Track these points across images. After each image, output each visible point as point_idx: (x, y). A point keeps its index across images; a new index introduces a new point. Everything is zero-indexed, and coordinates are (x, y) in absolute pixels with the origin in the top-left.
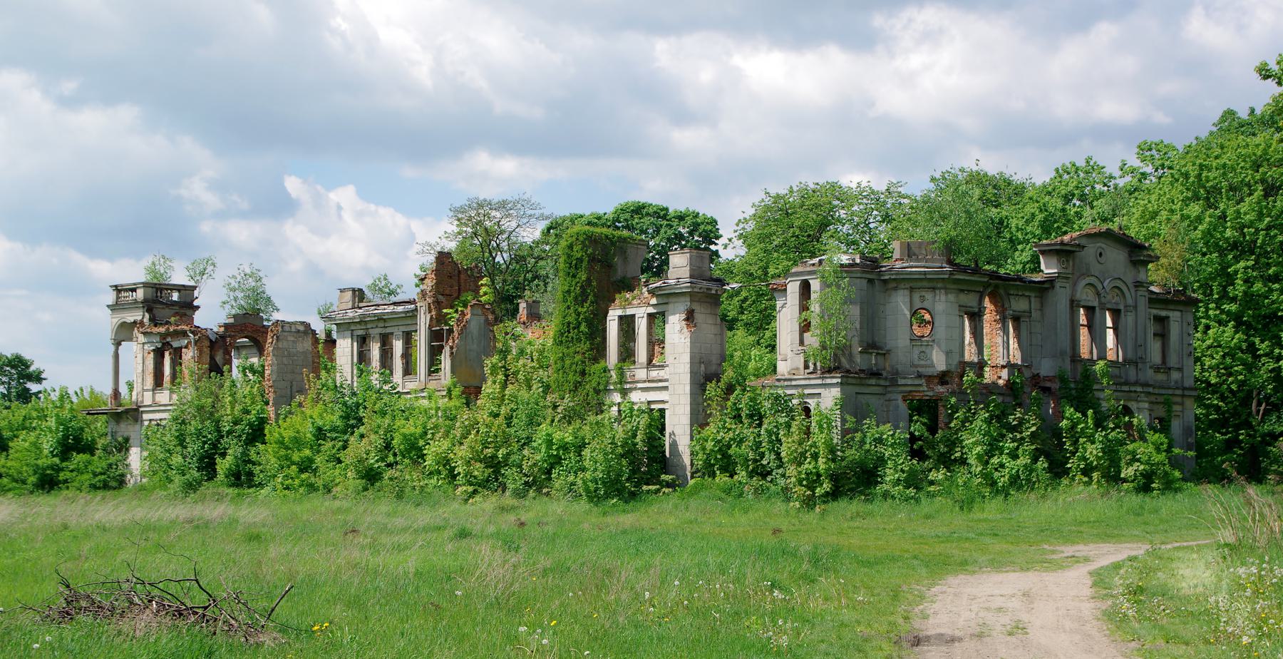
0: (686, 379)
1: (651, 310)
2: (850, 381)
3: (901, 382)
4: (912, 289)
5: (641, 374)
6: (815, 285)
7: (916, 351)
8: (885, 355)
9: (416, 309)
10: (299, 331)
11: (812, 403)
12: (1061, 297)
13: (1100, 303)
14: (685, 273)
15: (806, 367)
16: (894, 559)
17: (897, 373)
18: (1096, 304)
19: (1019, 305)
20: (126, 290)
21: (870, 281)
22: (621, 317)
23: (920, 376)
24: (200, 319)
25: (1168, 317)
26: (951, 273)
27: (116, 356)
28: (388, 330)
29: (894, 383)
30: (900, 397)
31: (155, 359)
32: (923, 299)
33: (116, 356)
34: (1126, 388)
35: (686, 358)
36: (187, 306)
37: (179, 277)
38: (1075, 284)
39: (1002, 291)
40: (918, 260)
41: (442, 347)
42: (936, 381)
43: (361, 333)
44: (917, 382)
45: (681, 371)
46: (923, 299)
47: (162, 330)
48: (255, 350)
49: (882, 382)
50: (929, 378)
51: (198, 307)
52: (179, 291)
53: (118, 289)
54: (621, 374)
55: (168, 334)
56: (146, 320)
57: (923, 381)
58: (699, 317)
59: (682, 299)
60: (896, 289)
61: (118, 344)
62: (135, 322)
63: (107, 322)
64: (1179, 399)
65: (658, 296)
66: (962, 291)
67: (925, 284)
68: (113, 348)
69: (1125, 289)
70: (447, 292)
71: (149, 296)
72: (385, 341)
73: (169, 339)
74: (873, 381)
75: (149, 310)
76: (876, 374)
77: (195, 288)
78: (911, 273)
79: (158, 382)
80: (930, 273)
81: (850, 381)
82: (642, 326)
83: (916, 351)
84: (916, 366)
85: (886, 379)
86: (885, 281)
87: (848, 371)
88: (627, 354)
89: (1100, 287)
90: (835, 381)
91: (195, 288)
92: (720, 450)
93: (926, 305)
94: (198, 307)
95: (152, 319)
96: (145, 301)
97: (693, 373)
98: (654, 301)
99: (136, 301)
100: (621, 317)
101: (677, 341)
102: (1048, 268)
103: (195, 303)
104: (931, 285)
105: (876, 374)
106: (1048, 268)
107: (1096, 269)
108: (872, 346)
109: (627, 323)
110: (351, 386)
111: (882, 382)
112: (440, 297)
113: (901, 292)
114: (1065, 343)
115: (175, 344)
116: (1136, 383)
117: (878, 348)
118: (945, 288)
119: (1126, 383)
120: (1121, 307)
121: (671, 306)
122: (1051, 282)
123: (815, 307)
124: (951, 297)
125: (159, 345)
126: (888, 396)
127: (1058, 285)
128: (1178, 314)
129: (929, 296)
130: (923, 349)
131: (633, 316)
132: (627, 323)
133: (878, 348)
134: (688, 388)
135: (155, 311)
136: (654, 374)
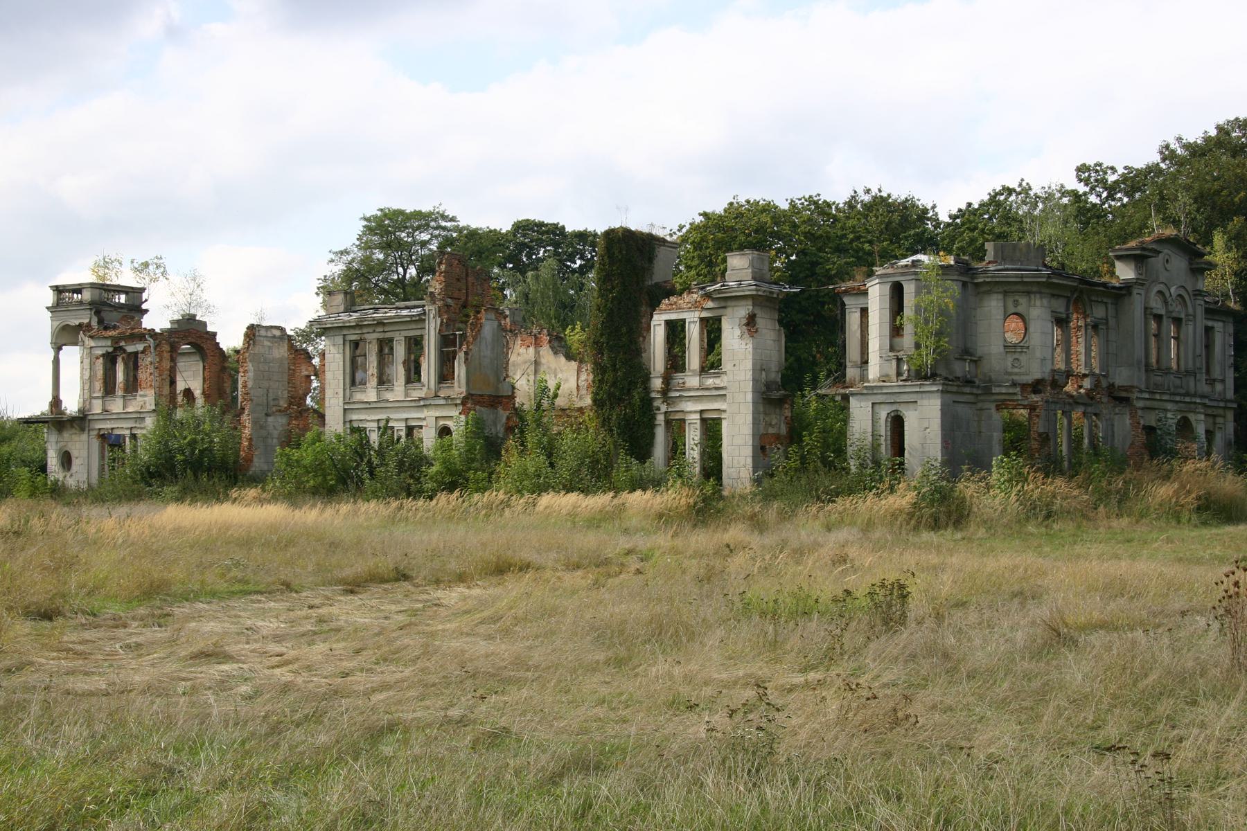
0: (749, 386)
1: (705, 314)
2: (950, 389)
3: (995, 390)
4: (1005, 293)
5: (693, 381)
6: (909, 289)
7: (1010, 359)
8: (976, 362)
9: (425, 314)
10: (274, 337)
11: (138, 432)
12: (1137, 303)
13: (1168, 312)
14: (747, 275)
15: (899, 374)
16: (525, 567)
17: (990, 381)
18: (1163, 312)
19: (1099, 312)
20: (69, 291)
21: (964, 284)
22: (668, 323)
23: (1014, 384)
24: (148, 322)
25: (1213, 328)
26: (1049, 277)
27: (56, 362)
28: (388, 335)
29: (987, 391)
30: (993, 406)
31: (105, 365)
32: (1016, 303)
33: (56, 362)
34: (1187, 399)
35: (748, 365)
36: (135, 308)
37: (127, 279)
38: (1147, 292)
39: (1085, 297)
40: (1012, 261)
41: (455, 353)
42: (1029, 389)
43: (354, 338)
44: (1011, 391)
45: (742, 378)
46: (1016, 303)
47: (113, 333)
48: (198, 358)
49: (975, 391)
50: (1024, 386)
51: (146, 311)
52: (126, 293)
53: (59, 290)
54: (667, 379)
55: (122, 337)
56: (94, 323)
57: (1018, 389)
58: (761, 322)
59: (743, 302)
60: (989, 292)
61: (58, 348)
62: (80, 325)
63: (45, 325)
64: (1221, 412)
65: (713, 300)
66: (1053, 295)
67: (1020, 288)
68: (52, 354)
69: (1186, 297)
70: (455, 295)
71: (97, 298)
72: (385, 346)
73: (122, 344)
74: (967, 390)
75: (98, 313)
76: (969, 382)
77: (143, 290)
78: (1007, 277)
79: (109, 388)
80: (1027, 276)
81: (950, 389)
82: (694, 333)
83: (1010, 359)
84: (1011, 374)
85: (978, 387)
86: (977, 285)
87: (946, 379)
88: (676, 362)
89: (1167, 295)
90: (935, 388)
91: (143, 290)
92: (710, 457)
93: (1020, 309)
94: (146, 311)
95: (100, 322)
96: (92, 303)
97: (755, 380)
98: (710, 304)
99: (81, 302)
100: (668, 323)
101: (736, 347)
102: (1125, 272)
103: (144, 306)
104: (1025, 288)
105: (969, 382)
106: (1125, 272)
107: (1163, 276)
108: (967, 353)
109: (675, 331)
110: (828, 376)
111: (975, 391)
112: (449, 301)
113: (995, 296)
114: (1139, 352)
115: (130, 349)
116: (1195, 395)
117: (971, 355)
118: (1040, 293)
119: (1187, 394)
120: (1183, 316)
121: (729, 310)
122: (1127, 287)
123: (909, 310)
124: (1045, 302)
125: (110, 350)
126: (980, 405)
127: (1135, 291)
128: (1221, 324)
129: (1023, 300)
130: (1017, 356)
131: (684, 321)
132: (675, 331)
133: (971, 355)
134: (750, 397)
135: (103, 314)
136: (710, 382)
